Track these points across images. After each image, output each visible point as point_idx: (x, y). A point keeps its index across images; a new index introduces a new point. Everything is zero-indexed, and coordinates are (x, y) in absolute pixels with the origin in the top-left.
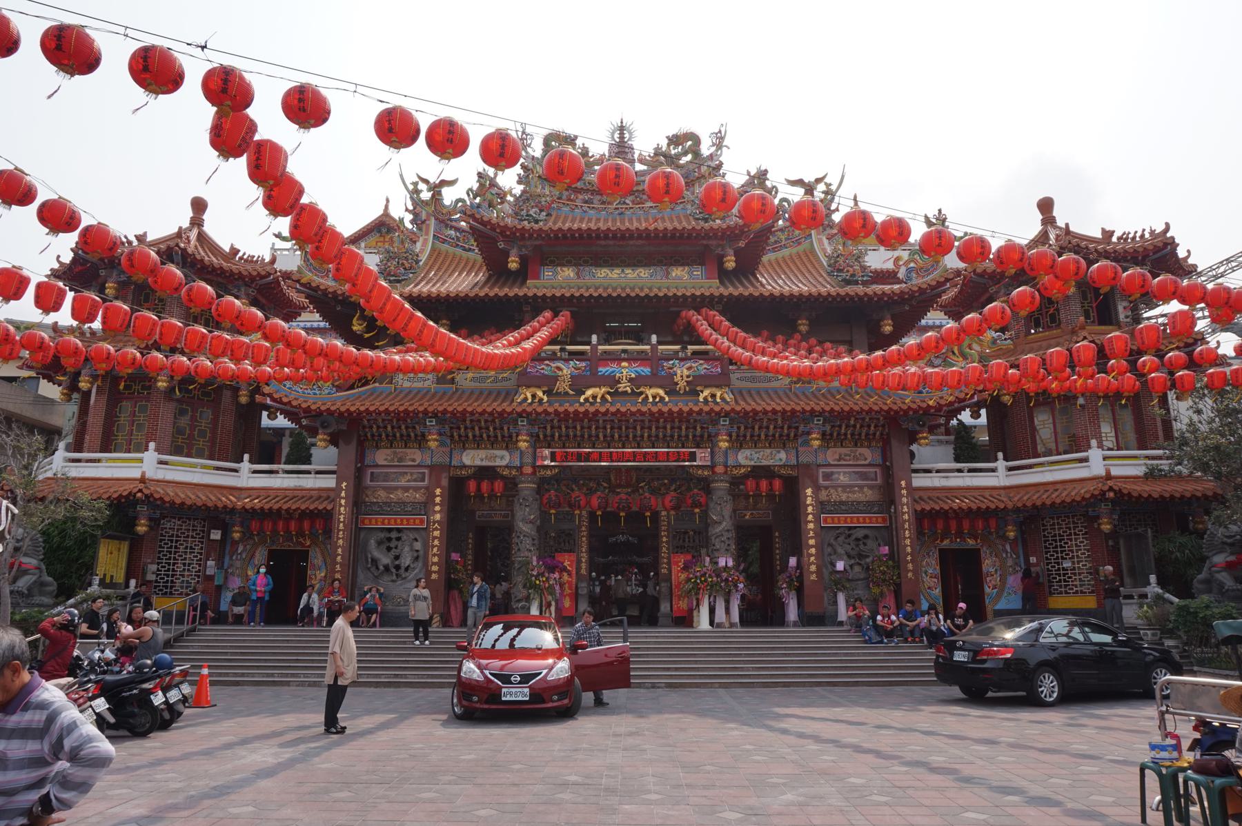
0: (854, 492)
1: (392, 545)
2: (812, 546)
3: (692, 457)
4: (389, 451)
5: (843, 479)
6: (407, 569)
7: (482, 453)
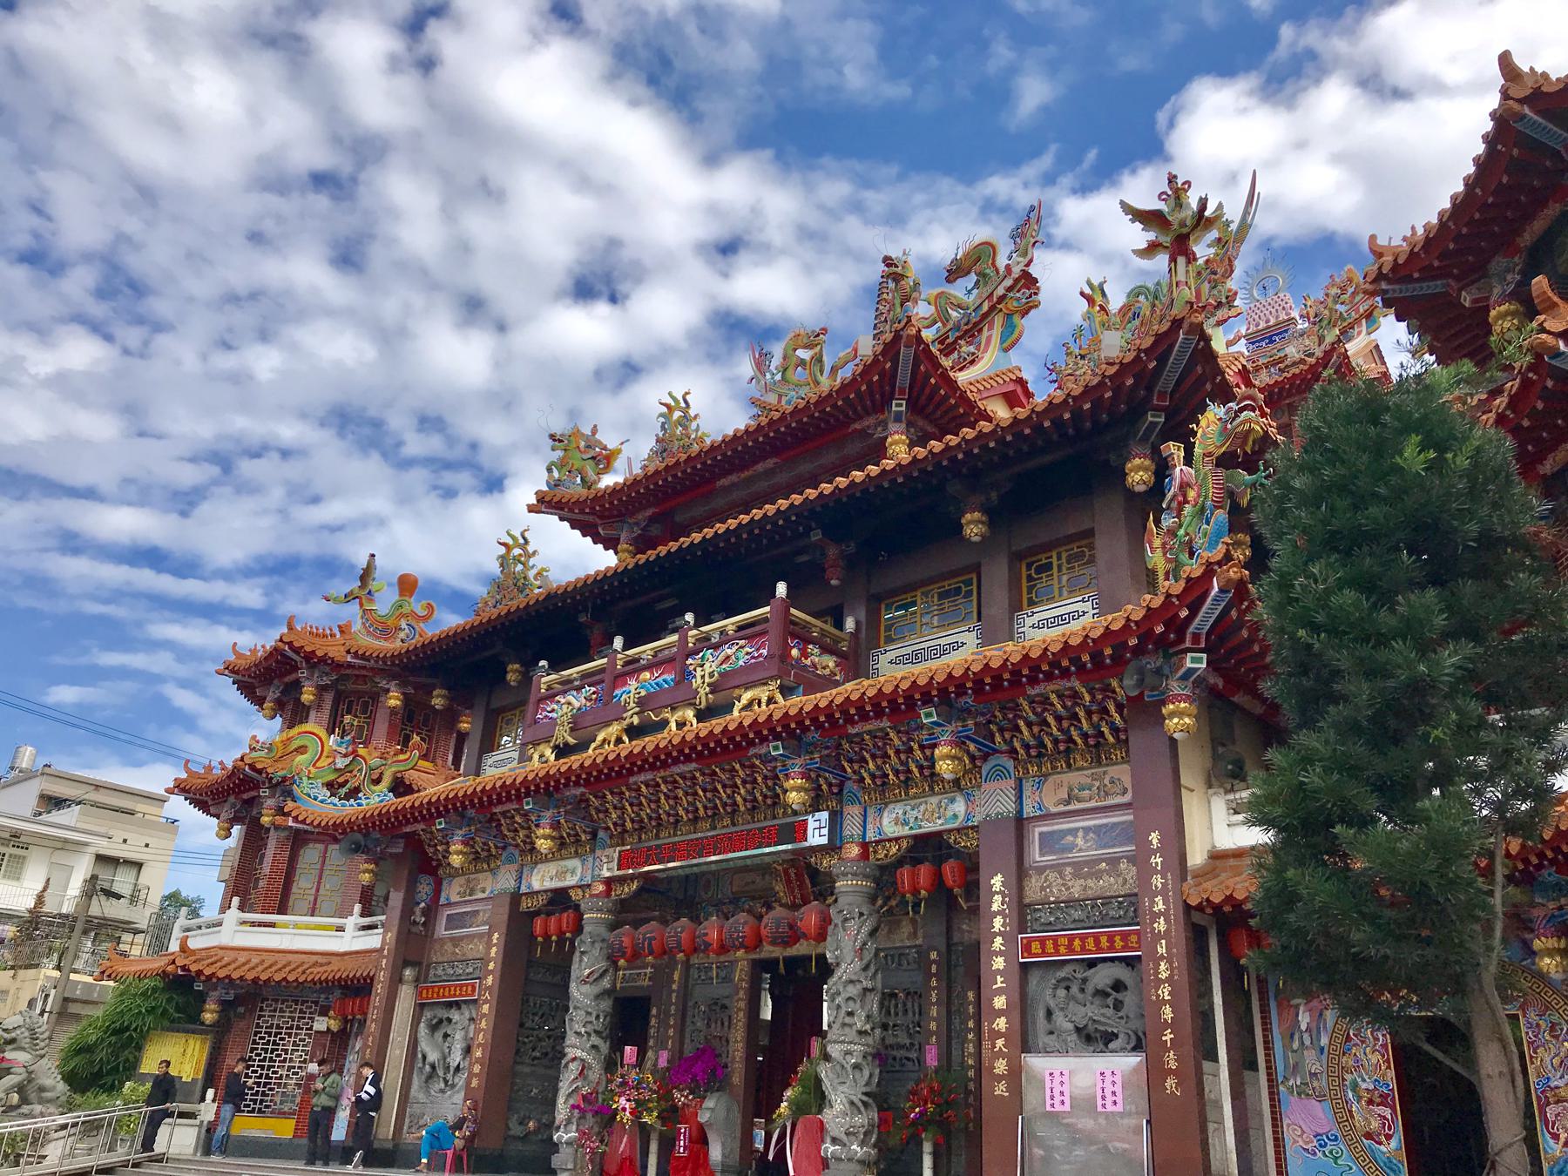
0: (1098, 875)
2: (1000, 1013)
5: (1084, 849)
6: (458, 1069)
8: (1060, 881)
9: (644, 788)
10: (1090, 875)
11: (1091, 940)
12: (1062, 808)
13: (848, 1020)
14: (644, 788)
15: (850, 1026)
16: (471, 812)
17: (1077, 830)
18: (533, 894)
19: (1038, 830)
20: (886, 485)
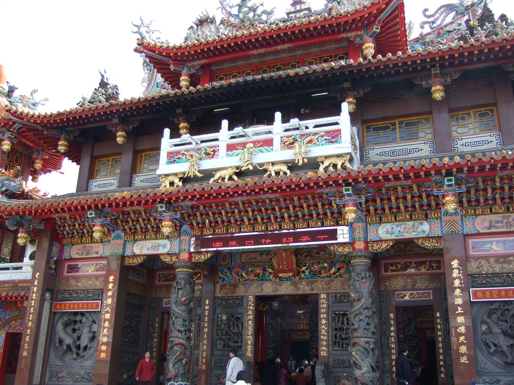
1: (76, 327)
3: (333, 235)
4: (79, 246)
6: (85, 348)
7: (149, 244)
8: (487, 264)
9: (132, 215)
10: (504, 262)
11: (76, 305)
12: (486, 231)
13: (367, 327)
14: (132, 215)
15: (368, 330)
16: (107, 209)
17: (492, 242)
18: (135, 256)
19: (67, 264)
20: (296, 81)
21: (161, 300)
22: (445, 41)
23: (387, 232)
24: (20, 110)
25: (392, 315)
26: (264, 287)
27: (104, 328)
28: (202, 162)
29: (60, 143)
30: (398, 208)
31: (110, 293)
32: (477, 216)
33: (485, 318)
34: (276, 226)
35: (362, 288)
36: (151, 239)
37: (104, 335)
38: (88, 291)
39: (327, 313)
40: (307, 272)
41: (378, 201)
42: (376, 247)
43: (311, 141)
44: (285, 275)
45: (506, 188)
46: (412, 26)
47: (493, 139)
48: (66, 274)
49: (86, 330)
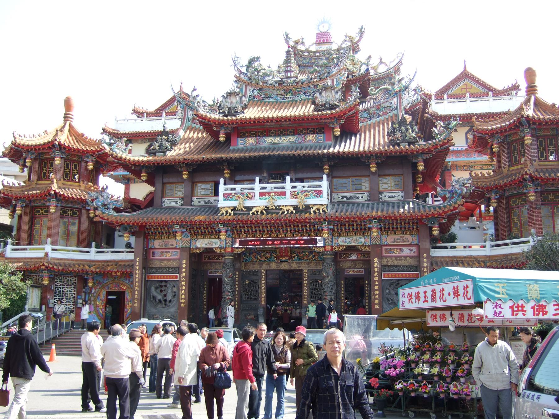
0: (402, 260)
3: (314, 242)
4: (160, 241)
6: (170, 301)
18: (197, 248)
21: (207, 271)
22: (381, 114)
23: (343, 241)
24: (119, 155)
25: (342, 282)
26: (271, 264)
27: (182, 290)
28: (245, 201)
29: (142, 174)
30: (349, 229)
31: (184, 270)
32: (388, 235)
33: (388, 287)
34: (283, 235)
35: (329, 272)
36: (207, 238)
37: (183, 294)
38: (168, 268)
39: (307, 280)
40: (296, 257)
41: (339, 225)
42: (337, 249)
43: (306, 195)
44: (284, 259)
45: (403, 223)
46: (363, 30)
47: (400, 194)
48: (151, 257)
49: (170, 291)
